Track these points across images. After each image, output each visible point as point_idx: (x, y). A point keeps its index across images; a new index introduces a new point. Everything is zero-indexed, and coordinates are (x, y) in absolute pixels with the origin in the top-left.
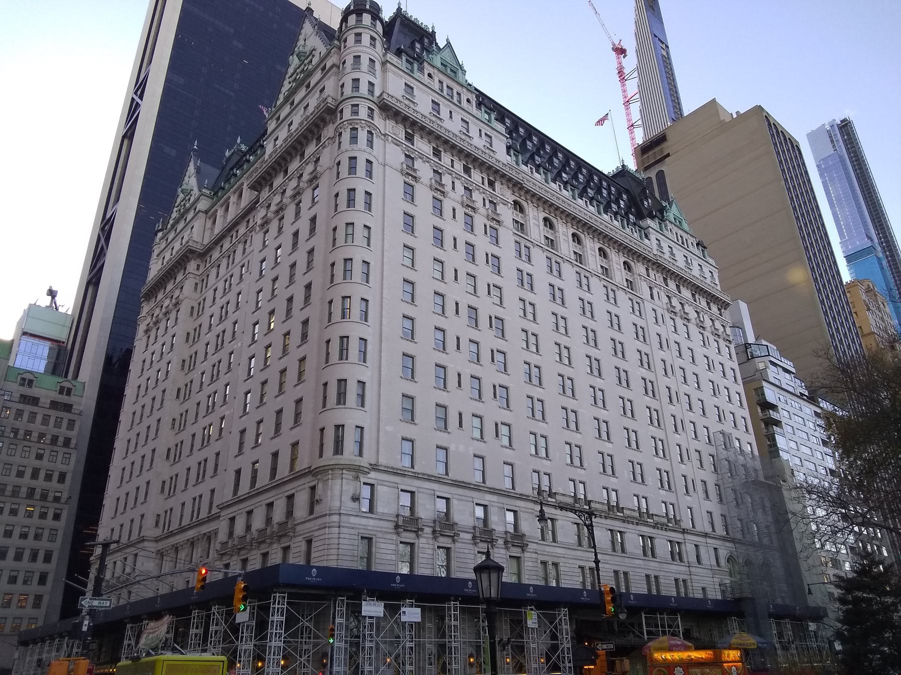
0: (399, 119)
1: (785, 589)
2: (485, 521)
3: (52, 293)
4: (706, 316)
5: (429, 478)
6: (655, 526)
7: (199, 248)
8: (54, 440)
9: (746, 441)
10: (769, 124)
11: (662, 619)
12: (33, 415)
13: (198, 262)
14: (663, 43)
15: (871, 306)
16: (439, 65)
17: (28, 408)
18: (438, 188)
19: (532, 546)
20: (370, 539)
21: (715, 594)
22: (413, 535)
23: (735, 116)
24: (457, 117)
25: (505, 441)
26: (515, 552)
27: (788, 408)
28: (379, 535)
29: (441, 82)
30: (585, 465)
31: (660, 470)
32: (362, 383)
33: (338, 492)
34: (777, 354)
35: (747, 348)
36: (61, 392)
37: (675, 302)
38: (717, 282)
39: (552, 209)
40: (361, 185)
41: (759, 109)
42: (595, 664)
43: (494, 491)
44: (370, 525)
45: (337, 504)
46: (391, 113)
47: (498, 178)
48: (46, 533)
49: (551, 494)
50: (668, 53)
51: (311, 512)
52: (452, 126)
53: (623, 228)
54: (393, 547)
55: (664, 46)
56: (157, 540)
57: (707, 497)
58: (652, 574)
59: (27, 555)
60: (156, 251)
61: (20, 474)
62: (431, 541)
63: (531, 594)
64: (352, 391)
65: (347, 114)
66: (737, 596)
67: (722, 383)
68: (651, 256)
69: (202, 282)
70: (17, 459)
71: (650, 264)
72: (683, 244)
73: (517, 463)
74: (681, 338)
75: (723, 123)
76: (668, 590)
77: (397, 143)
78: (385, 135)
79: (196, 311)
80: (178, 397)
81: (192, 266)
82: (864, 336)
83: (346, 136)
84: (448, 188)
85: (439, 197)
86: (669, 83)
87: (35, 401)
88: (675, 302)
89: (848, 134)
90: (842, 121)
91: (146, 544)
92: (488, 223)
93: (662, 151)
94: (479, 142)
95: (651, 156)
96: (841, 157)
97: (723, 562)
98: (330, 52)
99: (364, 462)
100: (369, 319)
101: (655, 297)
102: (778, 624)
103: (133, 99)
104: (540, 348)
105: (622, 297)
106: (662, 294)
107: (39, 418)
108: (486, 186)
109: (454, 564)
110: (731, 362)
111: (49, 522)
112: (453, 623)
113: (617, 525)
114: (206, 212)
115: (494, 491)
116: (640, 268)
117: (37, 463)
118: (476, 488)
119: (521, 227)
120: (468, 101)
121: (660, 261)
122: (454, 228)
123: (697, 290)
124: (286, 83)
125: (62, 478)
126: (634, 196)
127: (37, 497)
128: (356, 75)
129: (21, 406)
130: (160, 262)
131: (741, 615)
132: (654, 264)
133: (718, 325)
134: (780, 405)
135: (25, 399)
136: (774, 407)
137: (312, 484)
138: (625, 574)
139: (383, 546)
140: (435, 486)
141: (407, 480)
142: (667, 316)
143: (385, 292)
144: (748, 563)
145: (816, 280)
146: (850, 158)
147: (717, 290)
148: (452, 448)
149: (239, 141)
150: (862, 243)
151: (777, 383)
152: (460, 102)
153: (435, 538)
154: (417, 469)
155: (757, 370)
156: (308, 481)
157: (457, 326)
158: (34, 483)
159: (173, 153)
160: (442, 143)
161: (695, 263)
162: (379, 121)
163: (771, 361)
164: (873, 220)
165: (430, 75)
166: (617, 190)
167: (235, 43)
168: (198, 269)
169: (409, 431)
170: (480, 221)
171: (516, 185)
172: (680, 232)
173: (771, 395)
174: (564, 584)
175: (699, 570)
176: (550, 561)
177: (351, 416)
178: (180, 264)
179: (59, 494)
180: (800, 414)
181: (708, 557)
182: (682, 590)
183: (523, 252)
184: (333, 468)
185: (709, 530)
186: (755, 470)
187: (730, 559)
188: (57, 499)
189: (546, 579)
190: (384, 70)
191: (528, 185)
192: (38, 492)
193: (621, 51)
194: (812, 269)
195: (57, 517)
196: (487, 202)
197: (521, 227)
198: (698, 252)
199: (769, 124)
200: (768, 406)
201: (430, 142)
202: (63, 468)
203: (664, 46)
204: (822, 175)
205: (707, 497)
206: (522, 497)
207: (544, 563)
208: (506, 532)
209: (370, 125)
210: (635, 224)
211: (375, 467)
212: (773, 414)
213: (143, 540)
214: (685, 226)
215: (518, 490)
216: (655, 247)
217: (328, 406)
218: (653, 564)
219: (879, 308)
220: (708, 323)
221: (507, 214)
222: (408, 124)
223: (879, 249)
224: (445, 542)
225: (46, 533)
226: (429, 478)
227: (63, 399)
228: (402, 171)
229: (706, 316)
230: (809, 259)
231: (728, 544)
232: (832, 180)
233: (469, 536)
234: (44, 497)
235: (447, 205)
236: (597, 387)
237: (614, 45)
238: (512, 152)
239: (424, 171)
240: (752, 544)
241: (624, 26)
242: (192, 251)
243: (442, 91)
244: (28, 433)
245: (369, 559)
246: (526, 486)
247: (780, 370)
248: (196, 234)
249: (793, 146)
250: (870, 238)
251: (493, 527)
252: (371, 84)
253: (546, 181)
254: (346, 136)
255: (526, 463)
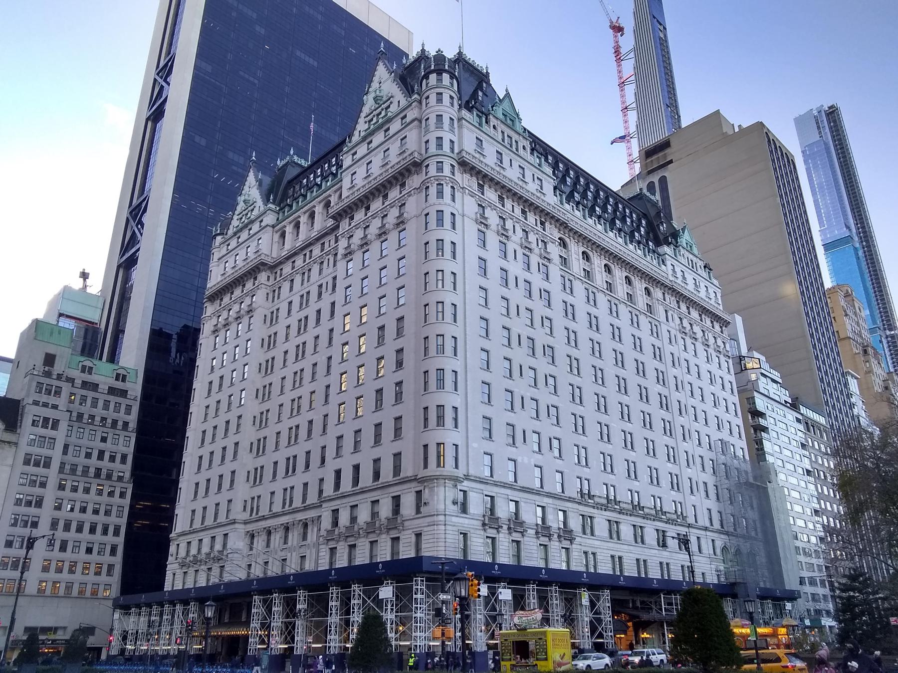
0: (468, 168)
1: (766, 574)
2: (517, 514)
3: (84, 276)
4: (710, 335)
5: (505, 485)
6: (667, 522)
7: (269, 260)
8: (115, 422)
9: (740, 446)
10: (769, 141)
11: (676, 599)
12: (95, 402)
13: (268, 273)
14: (661, 24)
15: (848, 312)
16: (501, 117)
17: (91, 394)
18: (504, 234)
19: (578, 539)
20: (465, 535)
21: (712, 579)
22: (495, 531)
23: (737, 130)
24: (515, 164)
25: (556, 453)
26: (566, 544)
27: (774, 415)
28: (472, 531)
29: (503, 132)
30: (615, 471)
31: (671, 474)
32: (455, 409)
33: (443, 498)
34: (766, 366)
35: (741, 360)
36: (83, 371)
37: (686, 323)
38: (720, 302)
39: (589, 244)
40: (448, 236)
41: (760, 125)
42: (625, 634)
43: (550, 495)
44: (464, 522)
45: (442, 507)
46: (468, 168)
47: (548, 219)
48: (114, 509)
49: (591, 496)
50: (665, 36)
51: (418, 511)
52: (511, 174)
53: (645, 256)
54: (482, 541)
55: (662, 28)
56: (246, 523)
57: (707, 496)
58: (665, 561)
59: (99, 529)
60: (216, 256)
61: (88, 455)
62: (507, 536)
63: (585, 579)
64: (449, 415)
65: (433, 170)
66: (732, 581)
67: (721, 394)
68: (668, 283)
69: (275, 292)
70: (85, 442)
71: (666, 289)
72: (693, 267)
73: (565, 471)
74: (689, 356)
75: (725, 136)
76: (655, 573)
77: (472, 195)
78: (462, 188)
79: (272, 318)
80: (257, 397)
81: (263, 277)
82: (841, 340)
83: (433, 190)
84: (511, 233)
85: (504, 241)
86: (665, 67)
87: (95, 387)
88: (686, 323)
89: (835, 121)
90: (830, 108)
91: (237, 526)
92: (541, 261)
93: (665, 156)
94: (532, 187)
95: (656, 160)
96: (826, 144)
97: (718, 551)
98: (411, 105)
99: (460, 473)
100: (458, 354)
101: (670, 318)
102: (762, 604)
103: (155, 80)
104: (581, 371)
105: (644, 320)
106: (676, 316)
107: (101, 404)
108: (539, 228)
109: (523, 554)
110: (729, 376)
111: (116, 499)
112: (555, 602)
113: (639, 521)
114: (273, 226)
115: (550, 495)
116: (658, 293)
117: (102, 446)
118: (538, 493)
119: (564, 261)
120: (524, 148)
121: (676, 286)
122: (515, 268)
123: (704, 311)
124: (361, 120)
125: (124, 458)
126: (646, 218)
127: (79, 473)
128: (439, 134)
129: (84, 392)
130: (222, 266)
131: (734, 596)
132: (670, 289)
133: (720, 342)
134: (768, 413)
135: (85, 385)
136: (762, 415)
137: (418, 489)
138: (645, 561)
139: (475, 539)
140: (508, 492)
141: (489, 487)
142: (679, 336)
143: (468, 329)
144: (738, 552)
145: (802, 293)
146: (835, 146)
147: (719, 310)
148: (519, 460)
149: (292, 152)
150: (840, 232)
151: (766, 393)
152: (517, 150)
153: (510, 533)
154: (496, 478)
155: (749, 381)
156: (414, 487)
157: (520, 355)
158: (100, 464)
159: (203, 142)
160: (506, 191)
161: (702, 285)
162: (458, 176)
163: (762, 374)
164: (852, 210)
165: (494, 127)
166: (638, 216)
167: (258, 28)
168: (268, 280)
169: (489, 446)
170: (535, 259)
171: (563, 225)
172: (691, 257)
173: (761, 404)
174: (600, 570)
175: (700, 558)
176: (590, 550)
177: (450, 436)
178: (250, 273)
179: (122, 474)
180: (784, 420)
181: (707, 547)
182: (592, 563)
183: (567, 287)
184: (437, 478)
185: (708, 524)
186: (746, 472)
187: (724, 549)
188: (120, 479)
189: (587, 566)
190: (460, 127)
191: (572, 225)
192: (104, 472)
193: (618, 29)
194: (800, 283)
195: (122, 495)
196: (540, 241)
197: (564, 261)
198: (705, 274)
199: (769, 141)
200: (757, 414)
201: (496, 191)
202: (125, 450)
203: (662, 28)
204: (806, 162)
205: (707, 496)
206: (570, 500)
207: (586, 553)
208: (559, 529)
209: (454, 181)
210: (654, 251)
211: (467, 477)
212: (762, 422)
213: (234, 523)
214: (695, 251)
215: (567, 494)
216: (670, 272)
217: (430, 427)
218: (665, 553)
219: (855, 314)
220: (711, 341)
221: (554, 250)
222: (480, 177)
223: (856, 239)
224: (516, 536)
225: (114, 509)
226: (505, 485)
227: (119, 385)
228: (476, 220)
229: (710, 335)
230: (798, 273)
231: (722, 536)
232: (816, 167)
233: (533, 532)
234: (109, 477)
235: (511, 247)
236: (624, 403)
237: (612, 22)
238: (558, 192)
239: (493, 218)
240: (743, 537)
241: (624, 7)
242: (263, 264)
243: (503, 140)
244: (92, 417)
245: (494, 554)
246: (572, 491)
247: (769, 380)
248: (265, 248)
249: (788, 161)
250: (848, 227)
251: (550, 524)
252: (452, 142)
253: (584, 216)
254: (433, 190)
255: (573, 471)
